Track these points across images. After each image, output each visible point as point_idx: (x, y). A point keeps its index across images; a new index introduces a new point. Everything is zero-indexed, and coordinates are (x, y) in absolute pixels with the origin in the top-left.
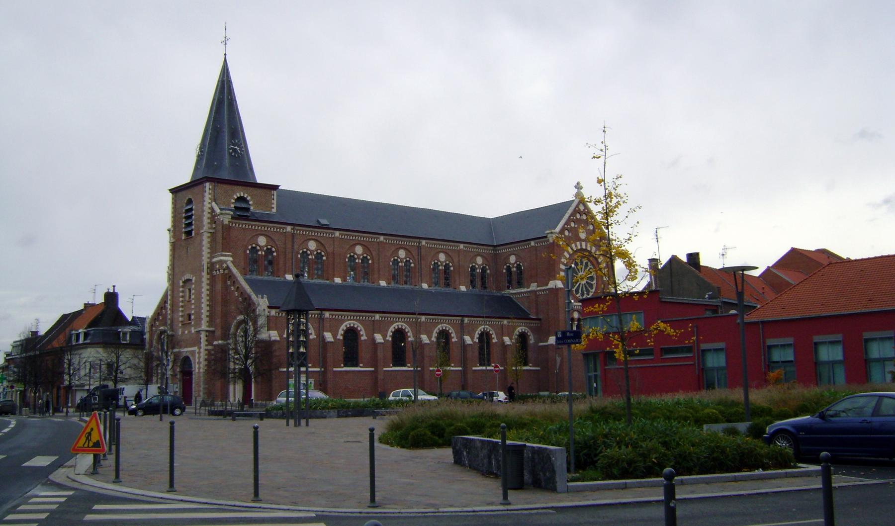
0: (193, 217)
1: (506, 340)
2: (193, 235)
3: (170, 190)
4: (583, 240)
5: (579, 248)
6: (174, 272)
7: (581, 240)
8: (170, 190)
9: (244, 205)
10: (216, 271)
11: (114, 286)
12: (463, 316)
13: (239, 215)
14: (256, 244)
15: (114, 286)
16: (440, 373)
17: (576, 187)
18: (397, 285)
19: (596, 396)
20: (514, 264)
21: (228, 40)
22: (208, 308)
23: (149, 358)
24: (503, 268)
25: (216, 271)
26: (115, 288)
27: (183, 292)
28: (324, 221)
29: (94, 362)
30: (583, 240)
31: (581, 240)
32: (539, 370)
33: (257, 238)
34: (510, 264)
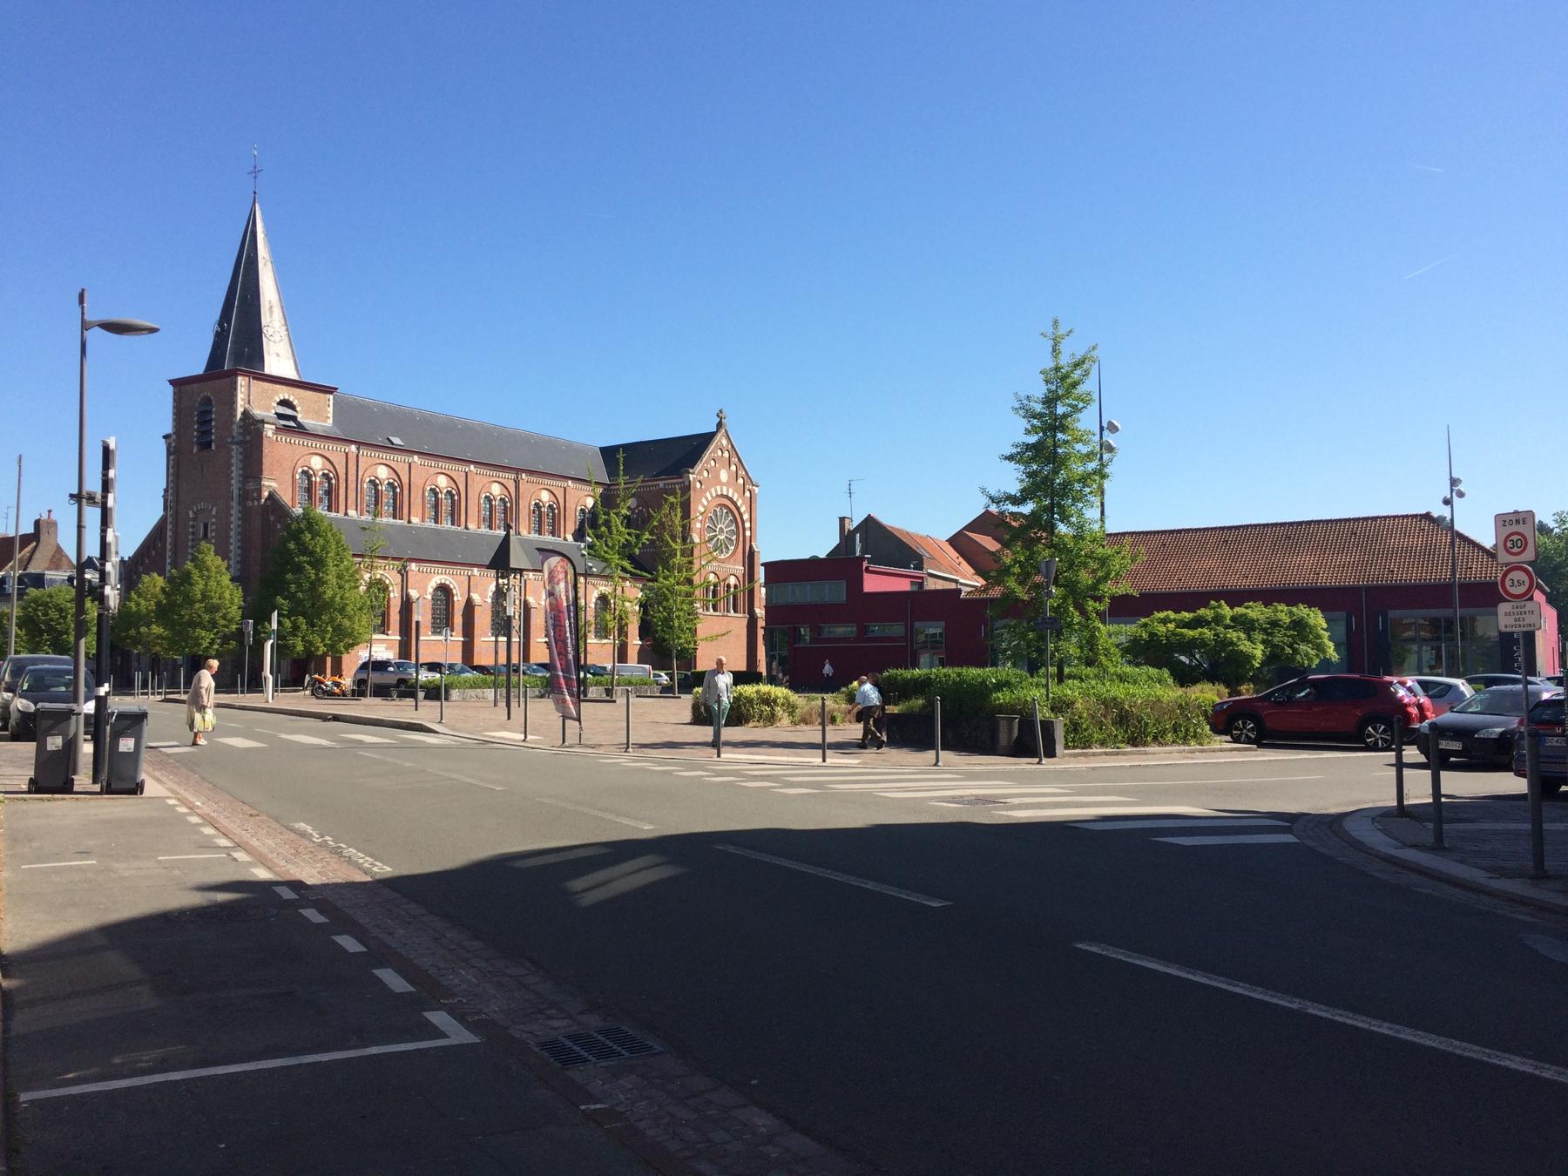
0: (213, 423)
1: (759, 615)
2: (213, 447)
3: (169, 381)
4: (724, 484)
6: (177, 498)
7: (721, 484)
8: (169, 381)
9: (289, 412)
10: (252, 501)
11: (50, 511)
13: (284, 426)
15: (50, 511)
17: (718, 415)
18: (395, 521)
19: (446, 699)
20: (635, 509)
22: (239, 551)
25: (252, 501)
26: (52, 513)
27: (193, 526)
29: (1311, 632)
30: (724, 484)
31: (721, 484)
33: (437, 477)
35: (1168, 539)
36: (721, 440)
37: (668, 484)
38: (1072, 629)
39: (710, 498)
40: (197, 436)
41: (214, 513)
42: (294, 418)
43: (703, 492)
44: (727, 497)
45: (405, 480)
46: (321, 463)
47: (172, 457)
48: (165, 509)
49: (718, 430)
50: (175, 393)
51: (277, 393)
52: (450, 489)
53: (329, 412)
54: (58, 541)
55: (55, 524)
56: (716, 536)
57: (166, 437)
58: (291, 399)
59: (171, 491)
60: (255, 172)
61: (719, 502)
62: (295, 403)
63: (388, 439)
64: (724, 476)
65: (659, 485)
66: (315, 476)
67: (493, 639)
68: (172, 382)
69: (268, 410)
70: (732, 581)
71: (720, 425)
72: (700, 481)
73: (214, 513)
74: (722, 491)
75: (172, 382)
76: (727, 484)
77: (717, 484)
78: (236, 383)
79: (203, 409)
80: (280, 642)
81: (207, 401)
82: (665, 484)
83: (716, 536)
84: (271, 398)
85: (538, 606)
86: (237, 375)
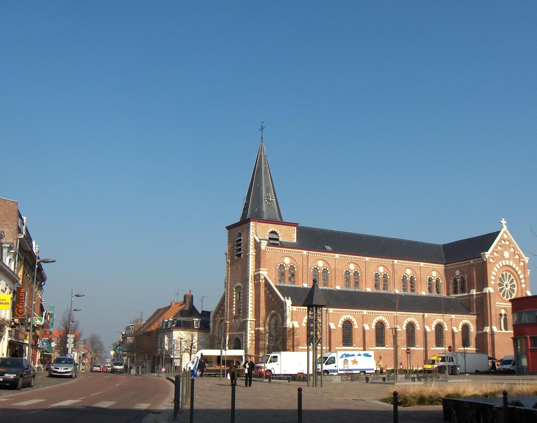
4: (507, 259)
9: (275, 236)
10: (257, 281)
11: (190, 291)
15: (190, 291)
30: (507, 259)
33: (284, 258)
34: (456, 276)
35: (510, 333)
39: (499, 267)
43: (494, 264)
44: (509, 266)
45: (363, 271)
46: (383, 269)
51: (268, 228)
53: (294, 236)
58: (276, 231)
60: (262, 128)
65: (470, 262)
66: (381, 275)
68: (228, 228)
70: (503, 312)
75: (228, 228)
76: (509, 259)
77: (503, 259)
78: (250, 225)
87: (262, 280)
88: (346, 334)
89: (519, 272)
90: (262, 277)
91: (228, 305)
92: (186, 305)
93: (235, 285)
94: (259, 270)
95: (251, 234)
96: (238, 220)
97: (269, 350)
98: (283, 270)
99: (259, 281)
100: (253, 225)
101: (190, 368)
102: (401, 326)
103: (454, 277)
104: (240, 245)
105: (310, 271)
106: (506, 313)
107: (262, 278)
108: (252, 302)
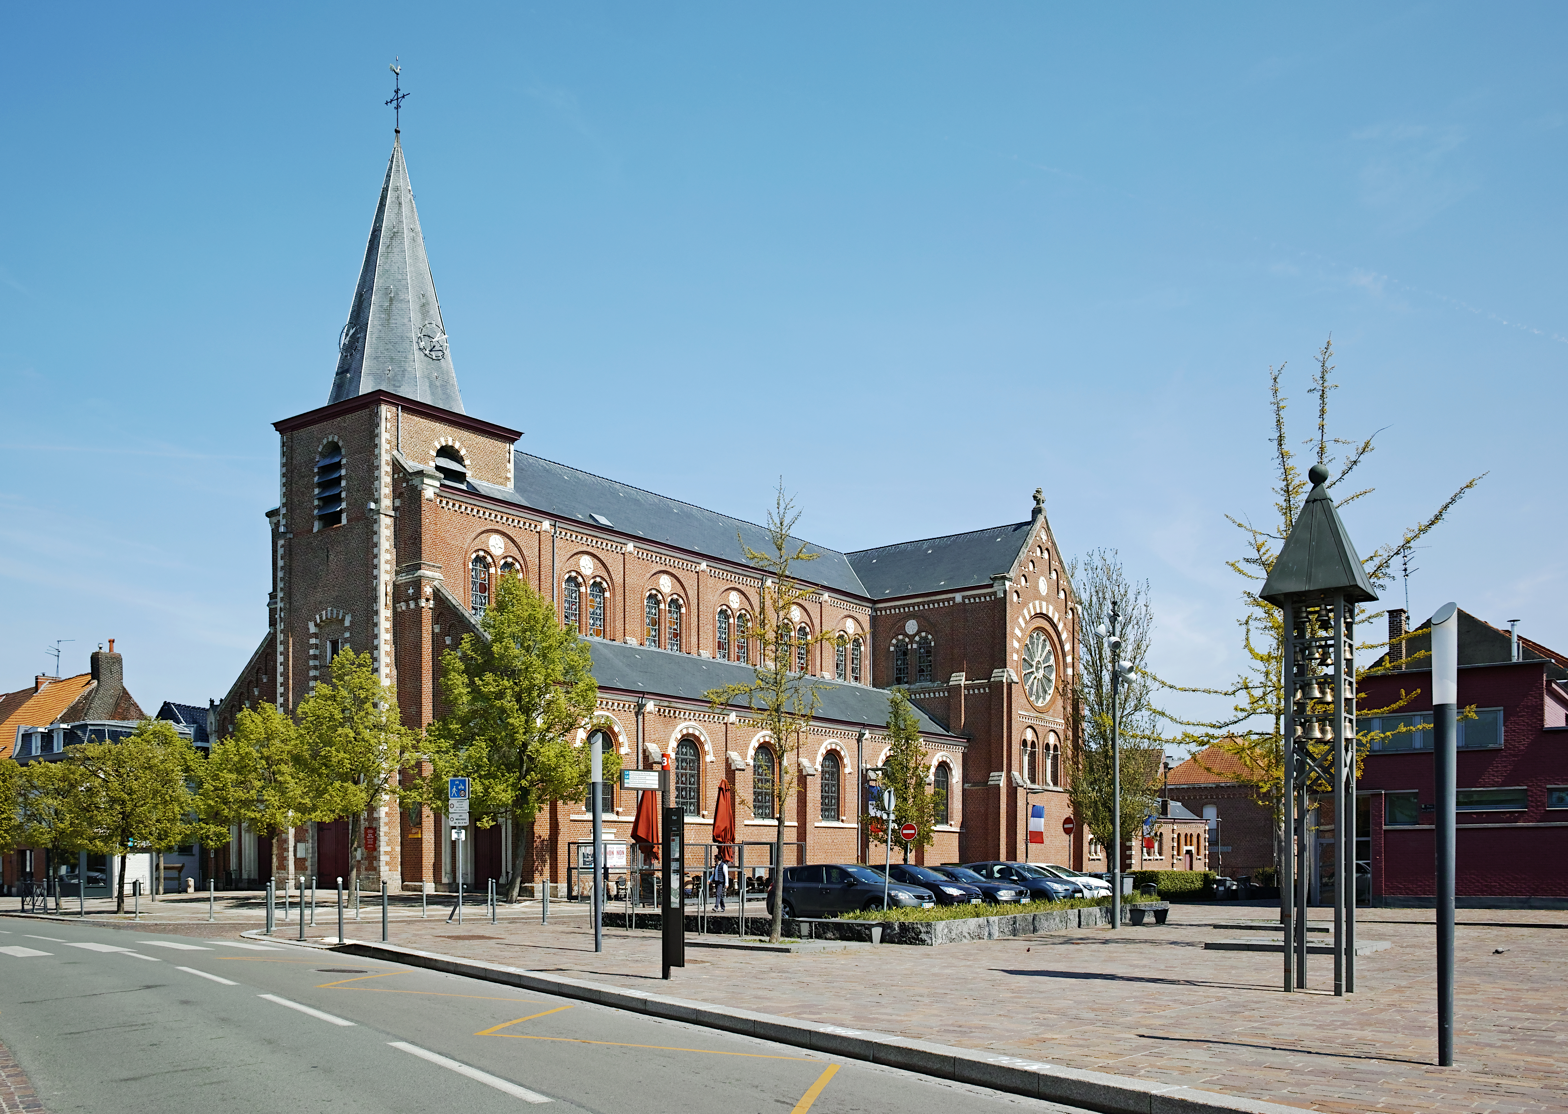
0: (343, 483)
2: (344, 521)
5: (1038, 611)
10: (407, 602)
11: (112, 642)
12: (864, 726)
14: (485, 551)
15: (112, 642)
16: (913, 832)
17: (1035, 497)
20: (915, 635)
21: (403, 97)
23: (69, 792)
24: (890, 644)
28: (603, 520)
31: (1041, 598)
32: (1432, 830)
33: (488, 538)
34: (906, 635)
36: (1038, 533)
37: (969, 597)
38: (131, 813)
40: (319, 507)
41: (347, 623)
42: (460, 477)
45: (618, 578)
47: (281, 542)
48: (272, 623)
49: (1034, 519)
50: (283, 444)
52: (675, 597)
54: (125, 685)
55: (117, 660)
56: (1032, 673)
57: (269, 515)
59: (280, 595)
60: (397, 99)
61: (1038, 625)
62: (463, 452)
63: (591, 516)
64: (1043, 586)
67: (589, 816)
68: (279, 426)
69: (424, 461)
70: (1052, 739)
71: (1036, 512)
72: (1016, 592)
73: (347, 623)
74: (1041, 608)
75: (279, 426)
76: (1047, 599)
78: (377, 414)
79: (327, 462)
80: (1360, 862)
81: (335, 448)
82: (964, 598)
83: (1032, 673)
84: (428, 442)
85: (815, 773)
86: (379, 402)
87: (427, 600)
88: (684, 779)
89: (1064, 636)
90: (428, 590)
91: (291, 682)
92: (99, 681)
93: (318, 617)
94: (418, 567)
95: (384, 446)
96: (323, 401)
97: (53, 850)
98: (483, 576)
99: (417, 604)
100: (389, 417)
101: (1067, 821)
102: (813, 761)
103: (900, 637)
104: (323, 485)
105: (559, 585)
106: (1035, 740)
107: (428, 593)
108: (388, 672)
